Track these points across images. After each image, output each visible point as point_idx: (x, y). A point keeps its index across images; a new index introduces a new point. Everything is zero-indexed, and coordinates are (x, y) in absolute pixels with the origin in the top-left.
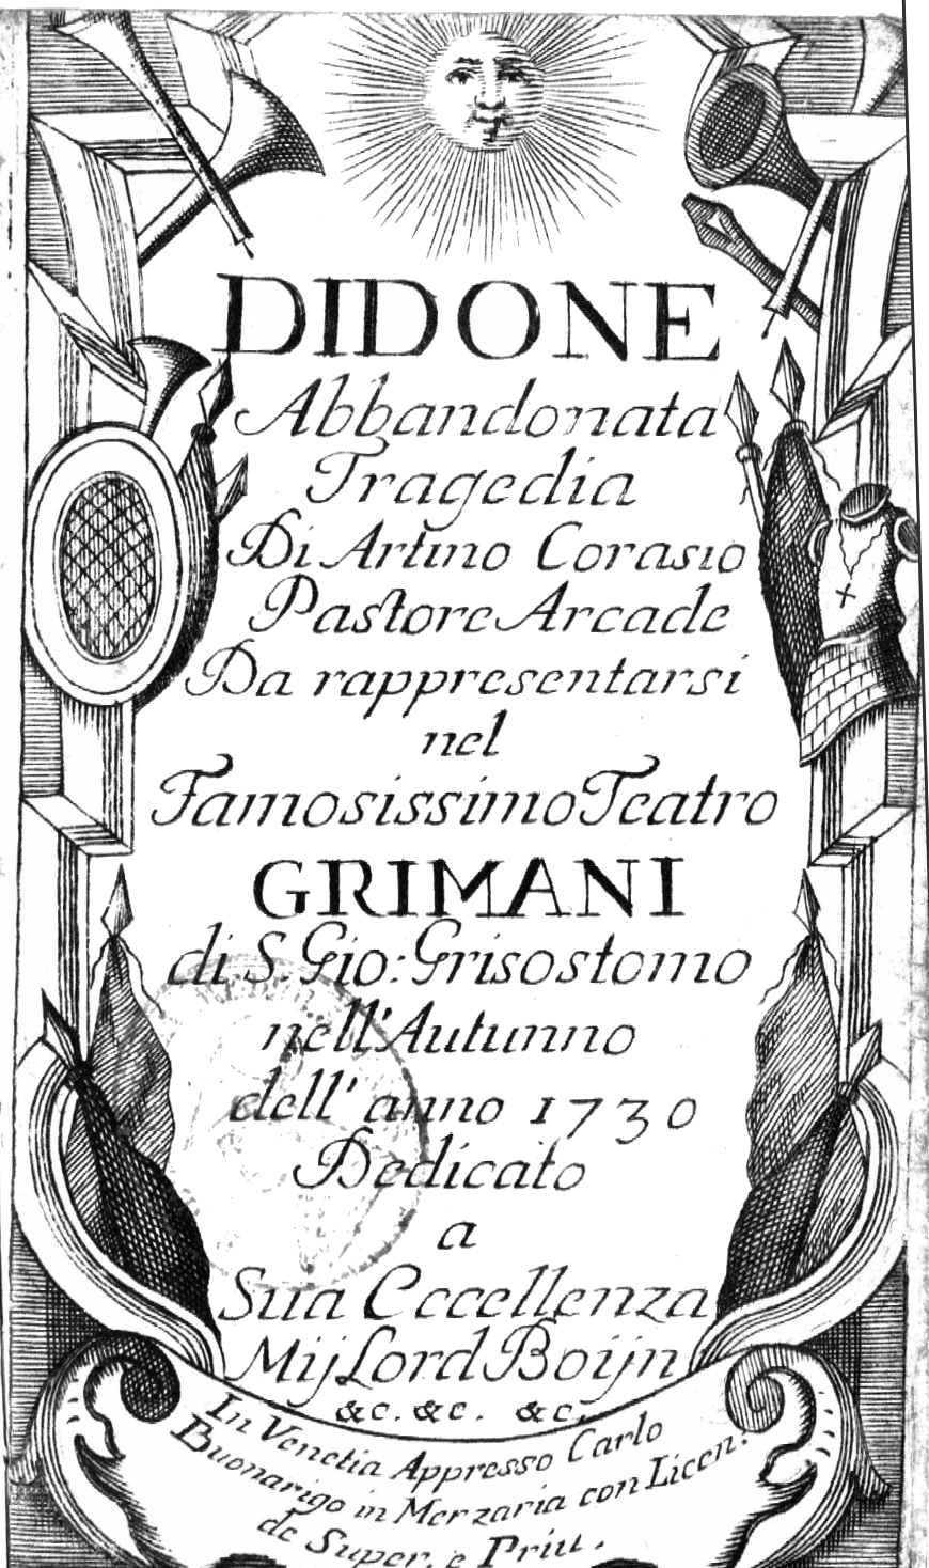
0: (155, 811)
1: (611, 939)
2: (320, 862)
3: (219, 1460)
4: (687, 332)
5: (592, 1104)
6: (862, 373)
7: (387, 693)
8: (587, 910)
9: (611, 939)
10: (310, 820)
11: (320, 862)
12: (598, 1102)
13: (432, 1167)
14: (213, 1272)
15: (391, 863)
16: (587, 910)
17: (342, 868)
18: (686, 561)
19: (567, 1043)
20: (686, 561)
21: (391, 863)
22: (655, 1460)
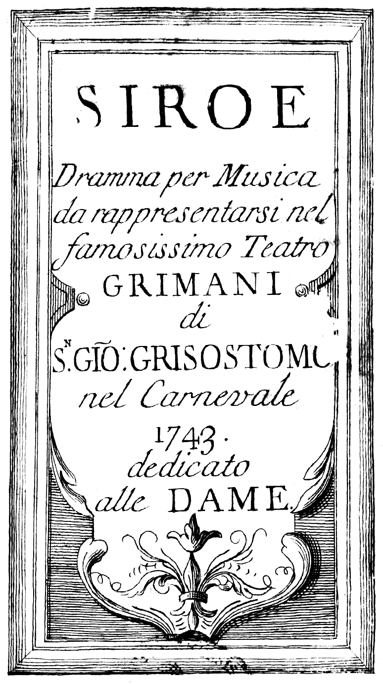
0: (164, 385)
1: (280, 501)
2: (121, 87)
3: (98, 246)
4: (156, 442)
5: (177, 428)
6: (253, 246)
7: (172, 463)
8: (238, 292)
9: (280, 501)
10: (162, 382)
11: (121, 87)
12: (179, 427)
13: (158, 356)
14: (96, 104)
15: (159, 370)
16: (238, 292)
17: (157, 348)
18: (176, 253)
19: (94, 218)
20: (176, 253)
21: (159, 370)
22: (169, 427)
